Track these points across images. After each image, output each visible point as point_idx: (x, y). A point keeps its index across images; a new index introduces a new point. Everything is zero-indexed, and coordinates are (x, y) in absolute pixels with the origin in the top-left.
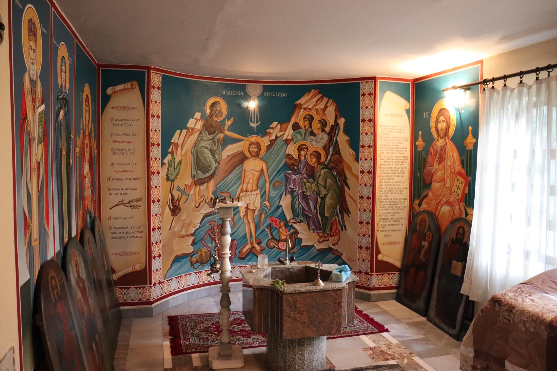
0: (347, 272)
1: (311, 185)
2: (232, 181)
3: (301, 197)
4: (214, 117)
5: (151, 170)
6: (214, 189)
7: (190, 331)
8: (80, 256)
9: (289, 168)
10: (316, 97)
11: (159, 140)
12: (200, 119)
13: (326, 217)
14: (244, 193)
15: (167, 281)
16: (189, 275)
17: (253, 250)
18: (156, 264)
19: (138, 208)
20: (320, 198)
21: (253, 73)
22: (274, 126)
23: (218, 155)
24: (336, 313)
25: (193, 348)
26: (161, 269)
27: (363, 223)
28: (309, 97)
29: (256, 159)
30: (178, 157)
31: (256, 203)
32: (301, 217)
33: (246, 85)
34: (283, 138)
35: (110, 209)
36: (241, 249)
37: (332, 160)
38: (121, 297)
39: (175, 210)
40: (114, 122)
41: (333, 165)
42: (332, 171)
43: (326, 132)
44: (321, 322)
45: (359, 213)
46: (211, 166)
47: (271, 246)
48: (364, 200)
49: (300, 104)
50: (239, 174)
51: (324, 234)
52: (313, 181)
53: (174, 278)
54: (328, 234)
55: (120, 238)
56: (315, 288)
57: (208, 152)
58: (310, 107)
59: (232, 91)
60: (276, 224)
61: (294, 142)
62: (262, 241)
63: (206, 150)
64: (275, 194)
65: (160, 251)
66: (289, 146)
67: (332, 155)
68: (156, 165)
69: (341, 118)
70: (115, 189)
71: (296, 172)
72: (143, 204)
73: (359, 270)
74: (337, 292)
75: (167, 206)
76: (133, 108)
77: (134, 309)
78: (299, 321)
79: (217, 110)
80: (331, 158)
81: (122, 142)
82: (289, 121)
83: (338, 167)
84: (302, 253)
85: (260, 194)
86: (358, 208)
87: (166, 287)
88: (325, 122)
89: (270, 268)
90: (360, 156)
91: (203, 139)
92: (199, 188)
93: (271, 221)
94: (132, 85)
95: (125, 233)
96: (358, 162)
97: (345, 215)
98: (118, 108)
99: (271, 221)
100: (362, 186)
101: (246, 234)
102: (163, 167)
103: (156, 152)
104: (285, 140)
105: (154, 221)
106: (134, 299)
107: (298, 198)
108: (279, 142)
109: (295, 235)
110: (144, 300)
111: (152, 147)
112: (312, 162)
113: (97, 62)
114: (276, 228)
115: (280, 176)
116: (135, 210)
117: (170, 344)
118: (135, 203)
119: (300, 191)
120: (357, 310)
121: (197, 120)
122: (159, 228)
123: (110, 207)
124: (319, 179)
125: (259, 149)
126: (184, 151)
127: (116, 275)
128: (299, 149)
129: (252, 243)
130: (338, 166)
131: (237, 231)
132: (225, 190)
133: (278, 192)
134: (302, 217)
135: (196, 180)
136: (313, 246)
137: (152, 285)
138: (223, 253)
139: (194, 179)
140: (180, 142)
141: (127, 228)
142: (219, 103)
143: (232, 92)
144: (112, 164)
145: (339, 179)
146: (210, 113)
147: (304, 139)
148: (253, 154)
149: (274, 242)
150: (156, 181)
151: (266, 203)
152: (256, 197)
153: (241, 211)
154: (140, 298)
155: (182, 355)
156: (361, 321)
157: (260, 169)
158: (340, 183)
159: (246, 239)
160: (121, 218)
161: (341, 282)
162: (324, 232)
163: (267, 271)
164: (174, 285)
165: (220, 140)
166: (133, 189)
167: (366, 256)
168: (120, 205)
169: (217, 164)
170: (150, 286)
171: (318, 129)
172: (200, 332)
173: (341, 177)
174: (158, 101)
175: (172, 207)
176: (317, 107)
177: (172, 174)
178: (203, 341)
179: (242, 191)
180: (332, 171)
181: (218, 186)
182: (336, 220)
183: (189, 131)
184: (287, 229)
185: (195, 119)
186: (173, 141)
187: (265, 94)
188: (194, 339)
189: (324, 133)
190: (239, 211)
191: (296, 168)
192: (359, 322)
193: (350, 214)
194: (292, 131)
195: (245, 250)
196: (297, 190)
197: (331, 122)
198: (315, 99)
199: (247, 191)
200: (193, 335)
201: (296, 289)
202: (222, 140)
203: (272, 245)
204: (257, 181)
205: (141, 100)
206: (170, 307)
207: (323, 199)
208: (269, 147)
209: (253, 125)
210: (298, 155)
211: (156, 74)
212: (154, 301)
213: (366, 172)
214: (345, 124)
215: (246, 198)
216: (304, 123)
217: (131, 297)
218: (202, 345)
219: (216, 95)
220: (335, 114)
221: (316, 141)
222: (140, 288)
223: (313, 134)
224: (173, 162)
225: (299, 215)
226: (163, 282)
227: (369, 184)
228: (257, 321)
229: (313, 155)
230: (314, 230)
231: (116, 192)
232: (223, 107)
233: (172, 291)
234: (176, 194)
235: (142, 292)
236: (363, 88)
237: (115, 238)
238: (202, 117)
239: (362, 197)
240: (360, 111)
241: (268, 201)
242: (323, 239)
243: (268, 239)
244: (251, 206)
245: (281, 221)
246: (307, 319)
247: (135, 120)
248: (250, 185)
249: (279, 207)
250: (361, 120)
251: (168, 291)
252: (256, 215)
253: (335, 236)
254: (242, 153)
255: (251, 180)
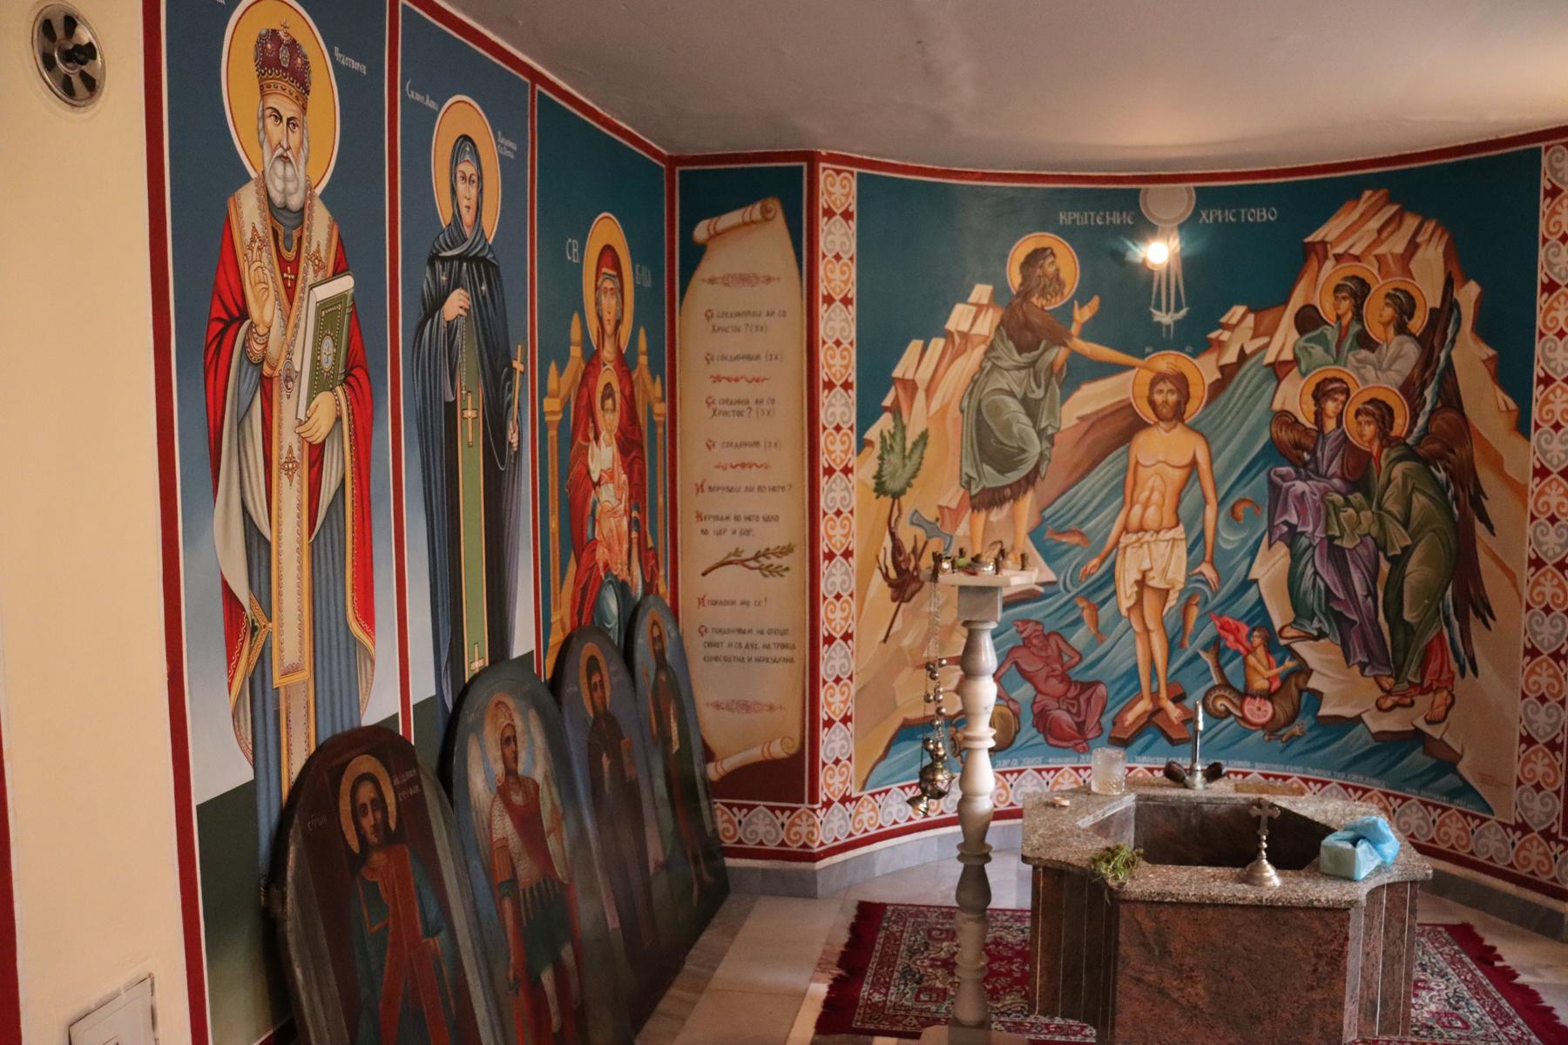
0: (1381, 846)
1: (1358, 513)
2: (1094, 497)
3: (1321, 554)
4: (1037, 295)
5: (823, 461)
6: (1035, 520)
7: (902, 962)
8: (532, 713)
9: (1284, 456)
10: (1380, 214)
11: (850, 370)
12: (988, 306)
13: (1407, 624)
14: (1134, 537)
15: (873, 795)
16: (883, 794)
17: (1157, 719)
18: (833, 743)
19: (782, 576)
20: (1388, 559)
21: (1146, 147)
22: (1234, 321)
23: (1048, 418)
24: (1319, 991)
25: (886, 1018)
26: (850, 759)
27: (1541, 654)
28: (1355, 215)
29: (1175, 426)
30: (916, 422)
31: (1171, 568)
32: (1320, 621)
33: (1138, 191)
34: (1265, 355)
35: (704, 574)
36: (1121, 711)
37: (1433, 429)
38: (728, 830)
39: (904, 584)
40: (714, 321)
41: (1437, 446)
42: (1433, 469)
43: (1412, 335)
44: (1258, 1018)
45: (1525, 617)
46: (1023, 451)
47: (1216, 710)
48: (1544, 575)
49: (1323, 243)
50: (1116, 475)
51: (1397, 683)
52: (1364, 502)
53: (894, 787)
54: (1412, 684)
55: (730, 661)
56: (1239, 895)
57: (1014, 405)
58: (1356, 251)
59: (1092, 214)
60: (1237, 641)
61: (1300, 369)
62: (1188, 692)
63: (1009, 400)
64: (1233, 542)
65: (849, 704)
66: (1284, 384)
67: (1432, 411)
68: (838, 448)
69: (1466, 281)
70: (717, 518)
71: (1307, 470)
72: (797, 563)
73: (1520, 820)
74: (1326, 915)
75: (877, 572)
76: (769, 280)
77: (764, 871)
78: (1176, 1001)
79: (1045, 275)
80: (1428, 421)
81: (737, 380)
82: (1286, 302)
83: (1454, 453)
84: (1321, 741)
85: (1186, 539)
86: (1521, 602)
87: (866, 815)
88: (1411, 298)
89: (1133, 796)
90: (1535, 415)
91: (1000, 368)
92: (987, 517)
93: (1222, 627)
94: (765, 211)
95: (744, 645)
96: (1528, 438)
97: (1475, 625)
98: (727, 280)
99: (1222, 627)
100: (1541, 524)
101: (1136, 666)
102: (862, 455)
103: (838, 408)
104: (1270, 365)
105: (831, 616)
106: (765, 841)
107: (1313, 556)
108: (1250, 375)
109: (1301, 681)
110: (794, 847)
111: (826, 392)
112: (1361, 436)
113: (663, 151)
114: (1237, 653)
115: (1254, 483)
116: (773, 581)
117: (829, 993)
118: (774, 561)
119: (1319, 534)
120: (1497, 964)
121: (980, 308)
122: (847, 637)
123: (703, 570)
124: (1385, 497)
125: (1185, 396)
126: (936, 404)
127: (716, 767)
128: (1320, 394)
129: (1155, 696)
130: (1452, 451)
131: (1112, 652)
132: (1072, 525)
133: (1243, 535)
134: (1324, 621)
135: (974, 491)
136: (1358, 719)
137: (819, 805)
138: (968, 734)
139: (969, 489)
140: (923, 376)
141: (750, 631)
142: (1053, 254)
143: (1095, 216)
144: (710, 444)
145: (1456, 497)
146: (1021, 285)
147: (1336, 362)
148: (1164, 410)
149: (1226, 697)
150: (838, 495)
151: (1206, 569)
152: (1172, 552)
153: (1121, 592)
154: (783, 840)
155: (844, 1036)
156: (1497, 1014)
157: (1187, 460)
158: (1457, 508)
159: (1136, 682)
160: (733, 603)
161: (1350, 879)
162: (1397, 676)
163: (1114, 807)
164: (894, 809)
165: (1056, 369)
166: (767, 519)
167: (1546, 775)
168: (730, 563)
169: (1046, 444)
170: (811, 806)
171: (1386, 325)
172: (932, 966)
173: (1463, 491)
174: (846, 253)
175: (893, 574)
176: (1382, 250)
177: (893, 475)
178: (926, 999)
179: (1126, 529)
180: (1433, 469)
181: (1047, 513)
182: (1440, 636)
183: (953, 343)
184: (1271, 659)
185: (973, 304)
186: (897, 373)
187: (1204, 215)
188: (902, 987)
189: (1404, 338)
190: (1114, 593)
191: (1306, 456)
192: (1491, 1012)
193: (1493, 618)
194: (1295, 335)
195: (1130, 717)
196: (1310, 529)
197: (1431, 296)
198: (1375, 224)
199: (1142, 529)
200: (907, 972)
201: (1170, 888)
202: (1061, 369)
203: (1222, 708)
204: (1175, 500)
205: (791, 253)
206: (878, 873)
207: (1398, 562)
208: (1217, 389)
209: (1164, 318)
210: (1316, 413)
211: (838, 172)
212: (821, 852)
213: (1555, 471)
214: (1480, 303)
215: (1140, 552)
216: (1336, 307)
217: (757, 833)
218: (917, 1013)
219: (1043, 228)
220: (1446, 268)
221: (1378, 367)
222: (783, 810)
223: (1365, 341)
224: (898, 438)
225: (1314, 615)
226: (858, 799)
227: (1541, 524)
228: (1041, 977)
229: (1367, 413)
230: (1363, 666)
231: (718, 525)
232: (1066, 264)
233: (889, 827)
234: (907, 534)
235: (787, 823)
236: (1551, 165)
237: (716, 659)
238: (995, 299)
239: (1537, 563)
240: (1537, 251)
241: (1212, 563)
242: (1396, 698)
243: (1209, 685)
244: (1153, 578)
245: (1254, 630)
246: (1207, 999)
247: (773, 313)
248: (1152, 510)
249: (1248, 583)
250: (1542, 283)
251: (871, 826)
252: (1170, 609)
253: (1436, 692)
254: (1126, 407)
255: (1156, 496)
